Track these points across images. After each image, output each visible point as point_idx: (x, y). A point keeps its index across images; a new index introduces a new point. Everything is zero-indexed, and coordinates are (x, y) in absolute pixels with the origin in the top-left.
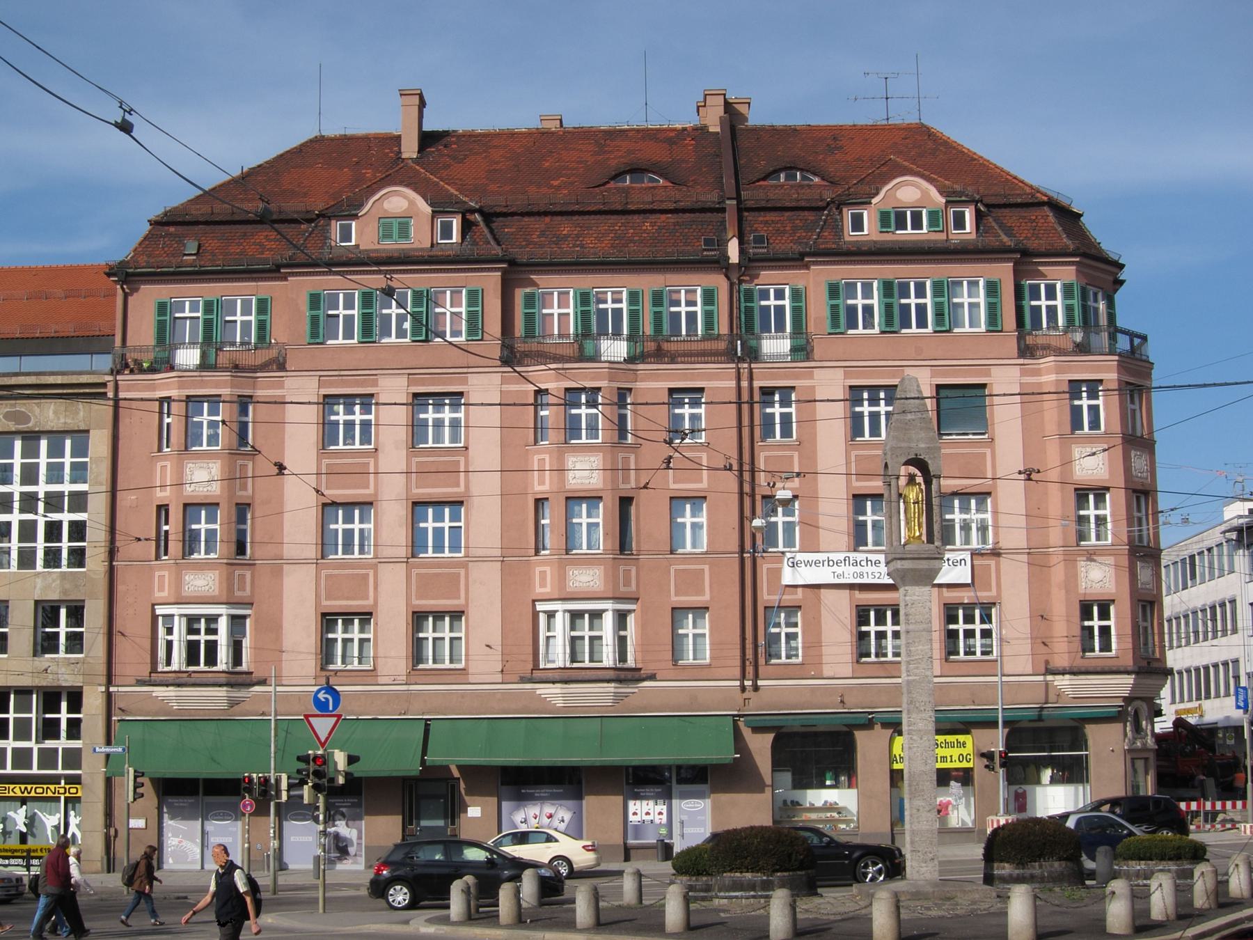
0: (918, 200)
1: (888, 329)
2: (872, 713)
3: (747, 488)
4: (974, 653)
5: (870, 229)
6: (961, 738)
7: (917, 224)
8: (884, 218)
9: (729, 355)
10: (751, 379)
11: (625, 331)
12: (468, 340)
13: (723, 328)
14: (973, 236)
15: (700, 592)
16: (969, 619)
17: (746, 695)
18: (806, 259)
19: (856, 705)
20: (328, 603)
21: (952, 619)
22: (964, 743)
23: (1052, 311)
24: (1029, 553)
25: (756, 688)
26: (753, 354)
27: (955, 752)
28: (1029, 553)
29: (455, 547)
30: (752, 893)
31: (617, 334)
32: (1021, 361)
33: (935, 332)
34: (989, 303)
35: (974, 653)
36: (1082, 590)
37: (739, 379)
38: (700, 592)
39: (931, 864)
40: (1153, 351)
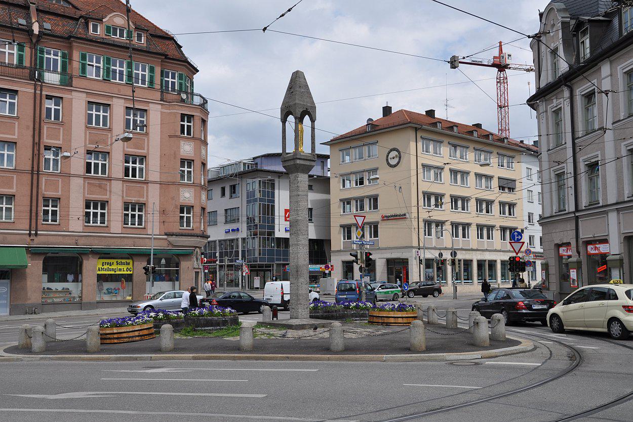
0: (122, 24)
1: (128, 82)
2: (91, 248)
3: (37, 140)
4: (135, 225)
5: (100, 32)
6: (128, 261)
7: (121, 35)
8: (108, 29)
9: (32, 78)
10: (41, 90)
11: (59, 70)
12: (127, 84)
13: (26, 63)
14: (145, 45)
15: (12, 188)
16: (133, 210)
17: (32, 238)
18: (72, 39)
19: (83, 244)
20: (89, 196)
21: (182, 212)
22: (129, 263)
23: (173, 83)
24: (160, 184)
25: (36, 234)
26: (40, 79)
27: (125, 267)
28: (160, 184)
29: (104, 172)
30: (218, 327)
31: (55, 71)
32: (162, 102)
33: (148, 87)
34: (150, 75)
35: (135, 225)
36: (181, 201)
37: (35, 90)
38: (12, 188)
39: (306, 310)
40: (209, 106)
